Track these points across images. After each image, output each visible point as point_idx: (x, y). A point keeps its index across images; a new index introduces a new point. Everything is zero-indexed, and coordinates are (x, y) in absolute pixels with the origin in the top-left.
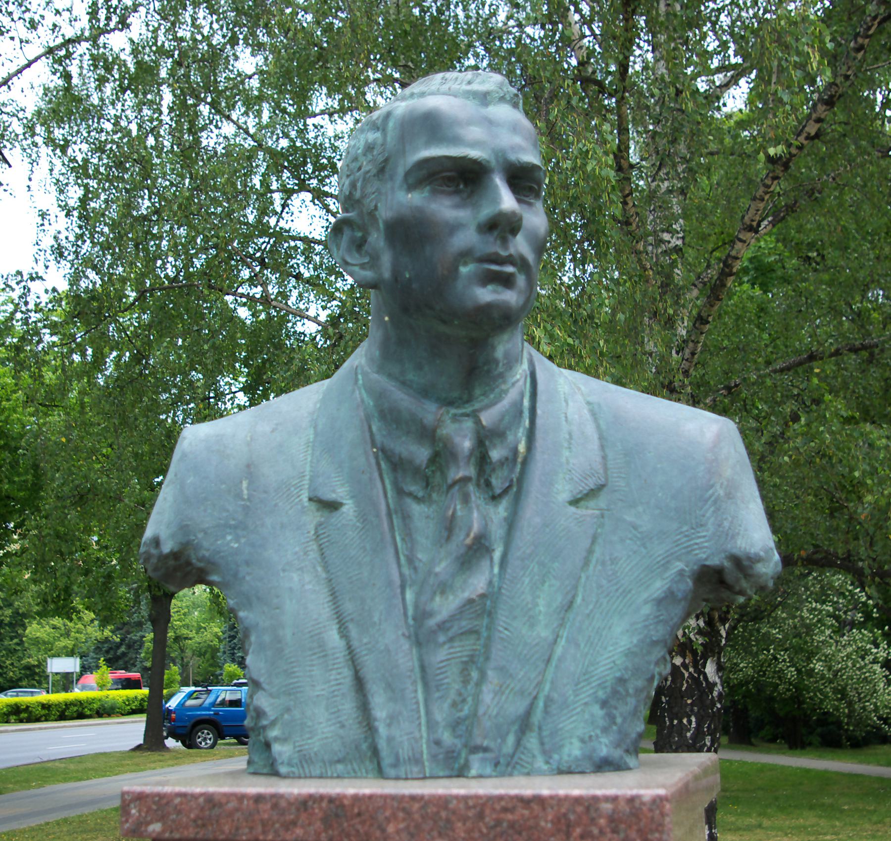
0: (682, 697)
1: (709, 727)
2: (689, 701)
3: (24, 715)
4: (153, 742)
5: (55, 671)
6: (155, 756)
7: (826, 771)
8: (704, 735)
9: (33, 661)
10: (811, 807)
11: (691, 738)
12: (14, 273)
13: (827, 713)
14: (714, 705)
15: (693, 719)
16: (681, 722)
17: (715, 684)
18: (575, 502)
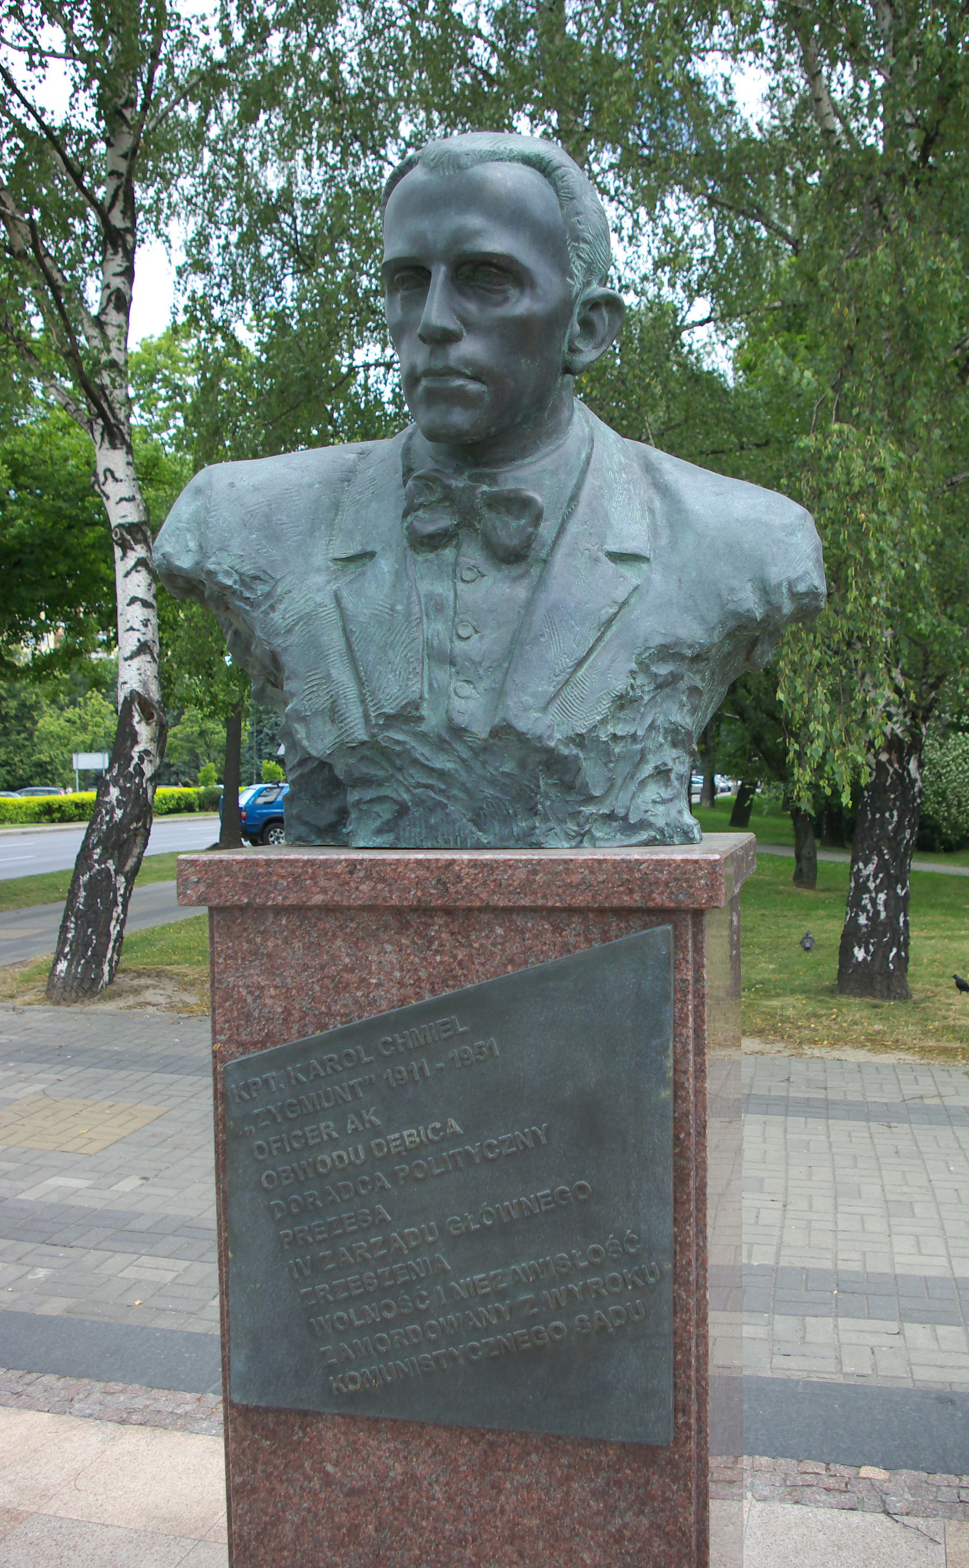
3: (57, 815)
7: (933, 873)
8: (905, 828)
9: (44, 758)
10: (933, 906)
12: (176, 279)
13: (929, 817)
16: (883, 815)
18: (372, 555)
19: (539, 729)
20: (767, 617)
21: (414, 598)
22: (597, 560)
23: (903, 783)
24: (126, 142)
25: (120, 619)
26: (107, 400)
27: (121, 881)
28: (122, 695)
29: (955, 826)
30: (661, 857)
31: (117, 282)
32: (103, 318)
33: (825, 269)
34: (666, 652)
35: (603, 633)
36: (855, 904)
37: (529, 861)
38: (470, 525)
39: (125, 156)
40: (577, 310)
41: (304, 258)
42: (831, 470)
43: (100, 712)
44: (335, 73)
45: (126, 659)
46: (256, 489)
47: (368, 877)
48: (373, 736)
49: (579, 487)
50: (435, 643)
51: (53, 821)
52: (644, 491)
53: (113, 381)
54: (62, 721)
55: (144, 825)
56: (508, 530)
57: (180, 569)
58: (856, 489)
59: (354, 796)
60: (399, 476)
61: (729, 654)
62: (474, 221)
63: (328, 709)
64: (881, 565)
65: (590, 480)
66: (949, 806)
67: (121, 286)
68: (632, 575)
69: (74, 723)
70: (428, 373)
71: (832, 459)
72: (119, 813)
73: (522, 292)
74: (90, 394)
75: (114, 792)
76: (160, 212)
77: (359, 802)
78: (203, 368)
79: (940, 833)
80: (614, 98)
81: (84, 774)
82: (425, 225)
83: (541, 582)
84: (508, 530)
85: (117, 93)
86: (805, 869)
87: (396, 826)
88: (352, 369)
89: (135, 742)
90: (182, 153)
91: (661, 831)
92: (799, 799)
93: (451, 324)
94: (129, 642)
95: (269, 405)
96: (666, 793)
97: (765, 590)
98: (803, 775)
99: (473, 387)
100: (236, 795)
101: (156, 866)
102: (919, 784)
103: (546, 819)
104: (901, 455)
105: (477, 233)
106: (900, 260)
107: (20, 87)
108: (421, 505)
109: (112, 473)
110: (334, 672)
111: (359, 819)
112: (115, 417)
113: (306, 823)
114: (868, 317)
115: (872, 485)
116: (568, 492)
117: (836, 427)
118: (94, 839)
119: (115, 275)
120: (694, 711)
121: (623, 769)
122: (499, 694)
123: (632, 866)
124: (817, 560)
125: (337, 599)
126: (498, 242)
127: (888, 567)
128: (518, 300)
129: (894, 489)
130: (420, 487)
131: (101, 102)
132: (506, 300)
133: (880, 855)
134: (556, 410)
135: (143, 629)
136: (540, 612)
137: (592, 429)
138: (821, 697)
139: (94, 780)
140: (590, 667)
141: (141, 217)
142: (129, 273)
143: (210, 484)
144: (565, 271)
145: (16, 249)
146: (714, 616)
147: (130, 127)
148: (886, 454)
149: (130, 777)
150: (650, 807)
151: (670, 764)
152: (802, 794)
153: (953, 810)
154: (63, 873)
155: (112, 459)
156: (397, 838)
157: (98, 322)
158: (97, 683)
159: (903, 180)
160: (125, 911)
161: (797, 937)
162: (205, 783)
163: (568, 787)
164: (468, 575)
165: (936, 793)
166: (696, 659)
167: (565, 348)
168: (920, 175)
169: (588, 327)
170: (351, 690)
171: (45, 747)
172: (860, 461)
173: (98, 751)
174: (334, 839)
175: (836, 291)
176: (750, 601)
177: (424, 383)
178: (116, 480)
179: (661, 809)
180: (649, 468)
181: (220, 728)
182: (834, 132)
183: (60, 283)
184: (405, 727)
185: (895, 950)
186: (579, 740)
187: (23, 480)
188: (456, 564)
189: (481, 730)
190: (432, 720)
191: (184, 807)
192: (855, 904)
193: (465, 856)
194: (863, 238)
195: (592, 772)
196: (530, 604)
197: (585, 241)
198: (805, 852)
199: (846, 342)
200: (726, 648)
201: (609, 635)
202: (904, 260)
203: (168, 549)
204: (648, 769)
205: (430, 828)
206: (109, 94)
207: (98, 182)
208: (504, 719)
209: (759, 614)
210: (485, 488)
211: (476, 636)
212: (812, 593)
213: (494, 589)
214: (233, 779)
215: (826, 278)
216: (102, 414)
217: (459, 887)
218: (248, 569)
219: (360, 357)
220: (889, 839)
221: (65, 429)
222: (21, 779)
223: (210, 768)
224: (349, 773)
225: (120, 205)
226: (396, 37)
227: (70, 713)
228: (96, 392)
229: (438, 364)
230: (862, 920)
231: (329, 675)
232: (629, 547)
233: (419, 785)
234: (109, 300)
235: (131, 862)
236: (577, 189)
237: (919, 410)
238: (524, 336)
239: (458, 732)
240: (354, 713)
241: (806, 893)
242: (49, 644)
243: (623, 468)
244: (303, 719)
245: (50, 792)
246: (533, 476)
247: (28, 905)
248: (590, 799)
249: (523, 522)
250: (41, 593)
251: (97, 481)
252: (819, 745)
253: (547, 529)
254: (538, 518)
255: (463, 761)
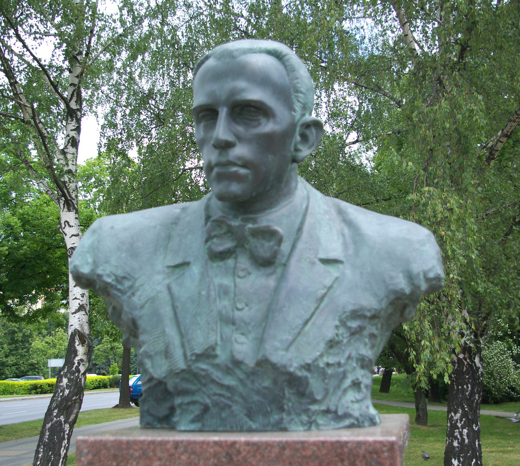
0: (463, 374)
1: (477, 390)
2: (467, 377)
3: (39, 390)
4: (124, 403)
5: (52, 366)
6: (127, 411)
8: (475, 394)
10: (491, 434)
11: (468, 395)
14: (479, 378)
15: (469, 386)
16: (463, 387)
17: (479, 368)
19: (284, 361)
20: (413, 293)
21: (212, 287)
22: (313, 263)
23: (473, 369)
24: (78, 70)
25: (70, 294)
26: (66, 188)
27: (67, 426)
28: (70, 331)
29: (499, 390)
30: (361, 438)
31: (73, 134)
32: (66, 150)
33: (416, 112)
34: (355, 314)
35: (319, 305)
36: (451, 435)
37: (280, 442)
38: (242, 246)
39: (77, 77)
40: (298, 129)
41: (160, 120)
42: (426, 210)
43: (62, 337)
44: (174, 36)
45: (73, 314)
46: (125, 229)
47: (186, 451)
48: (189, 366)
49: (302, 223)
50: (224, 312)
51: (37, 393)
52: (338, 224)
53: (70, 179)
54: (43, 343)
55: (80, 397)
56: (264, 248)
57: (83, 274)
58: (439, 219)
59: (178, 401)
60: (203, 221)
61: (391, 314)
62: (241, 84)
63: (163, 352)
64: (454, 258)
65: (309, 220)
66: (495, 380)
67: (75, 135)
68: (334, 271)
69: (50, 344)
70: (218, 164)
71: (425, 205)
72: (67, 392)
73: (268, 120)
74: (58, 186)
75: (65, 381)
76: (93, 102)
77: (180, 405)
78: (112, 173)
79: (491, 394)
80: (308, 39)
81: (54, 369)
82: (215, 87)
83: (282, 278)
84: (264, 248)
85: (74, 49)
86: (421, 415)
87: (203, 419)
88: (184, 170)
89: (76, 355)
90: (103, 75)
91: (357, 419)
92: (420, 381)
93: (230, 138)
94: (74, 305)
95: (144, 188)
96: (359, 396)
97: (410, 277)
98: (421, 368)
99: (243, 171)
100: (128, 380)
101: (87, 416)
102: (481, 370)
103: (289, 413)
104: (461, 201)
105: (243, 90)
106: (453, 107)
107: (30, 48)
108: (215, 236)
109: (68, 223)
110: (167, 330)
111: (181, 414)
112: (70, 196)
113: (151, 415)
114: (439, 134)
115: (447, 217)
116: (296, 226)
117: (426, 189)
118: (54, 405)
119: (72, 130)
120: (373, 347)
121: (333, 383)
122: (261, 341)
123: (341, 445)
124: (439, 260)
125: (169, 288)
126: (255, 94)
127: (458, 259)
128: (266, 124)
129: (459, 219)
130: (214, 226)
131: (67, 54)
132: (259, 124)
133: (463, 409)
134: (288, 183)
135: (81, 299)
136: (283, 294)
137: (308, 192)
138: (427, 327)
139: (57, 372)
140: (313, 324)
141: (84, 103)
142: (78, 129)
143: (100, 228)
144: (291, 108)
145: (26, 120)
146: (382, 293)
147: (80, 63)
148: (453, 201)
149: (73, 373)
150: (350, 404)
151: (360, 379)
152: (422, 378)
153: (497, 382)
154: (39, 420)
155: (68, 216)
156: (203, 425)
157: (63, 152)
158: (59, 325)
159: (452, 69)
160: (68, 442)
161: (419, 453)
162: (113, 373)
163: (302, 394)
164: (241, 274)
165: (488, 373)
166: (373, 317)
167: (292, 149)
168: (460, 65)
169: (304, 138)
170: (176, 340)
171: (35, 356)
172: (440, 205)
173: (61, 358)
174: (167, 424)
175: (422, 123)
176: (402, 284)
177: (216, 170)
178: (70, 226)
179: (356, 406)
180: (341, 212)
181: (121, 345)
182: (415, 49)
183: (46, 135)
184: (207, 361)
185: (474, 460)
186: (308, 367)
187: (27, 227)
188: (235, 268)
189: (250, 362)
190: (222, 356)
191: (101, 386)
192: (451, 435)
193: (242, 438)
194: (434, 97)
195: (315, 385)
196: (277, 290)
197: (301, 92)
198: (420, 406)
199: (429, 147)
200: (390, 311)
201: (322, 305)
202: (455, 106)
203: (77, 263)
204: (348, 382)
205: (223, 420)
206: (70, 49)
207: (65, 89)
208: (264, 356)
209: (407, 291)
210: (250, 226)
211: (247, 308)
212: (438, 278)
213: (257, 281)
214: (126, 372)
215: (416, 117)
216: (64, 195)
217: (240, 457)
218: (120, 273)
219: (188, 165)
220: (467, 399)
221: (47, 203)
222: (23, 372)
223: (115, 366)
224: (175, 387)
225: (74, 99)
226: (203, 19)
227: (48, 339)
228: (61, 184)
229: (223, 159)
230: (456, 444)
231: (164, 332)
232: (332, 255)
233: (215, 394)
234: (69, 142)
235: (72, 417)
236: (296, 66)
237: (469, 178)
238: (270, 143)
239: (237, 363)
240: (178, 353)
241: (423, 428)
242: (39, 305)
243: (326, 212)
244: (150, 357)
245: (36, 379)
246: (277, 218)
247: (22, 437)
248: (315, 401)
249: (272, 243)
250: (34, 282)
251: (61, 227)
252: (427, 352)
253: (285, 247)
254: (280, 241)
255: (241, 381)
